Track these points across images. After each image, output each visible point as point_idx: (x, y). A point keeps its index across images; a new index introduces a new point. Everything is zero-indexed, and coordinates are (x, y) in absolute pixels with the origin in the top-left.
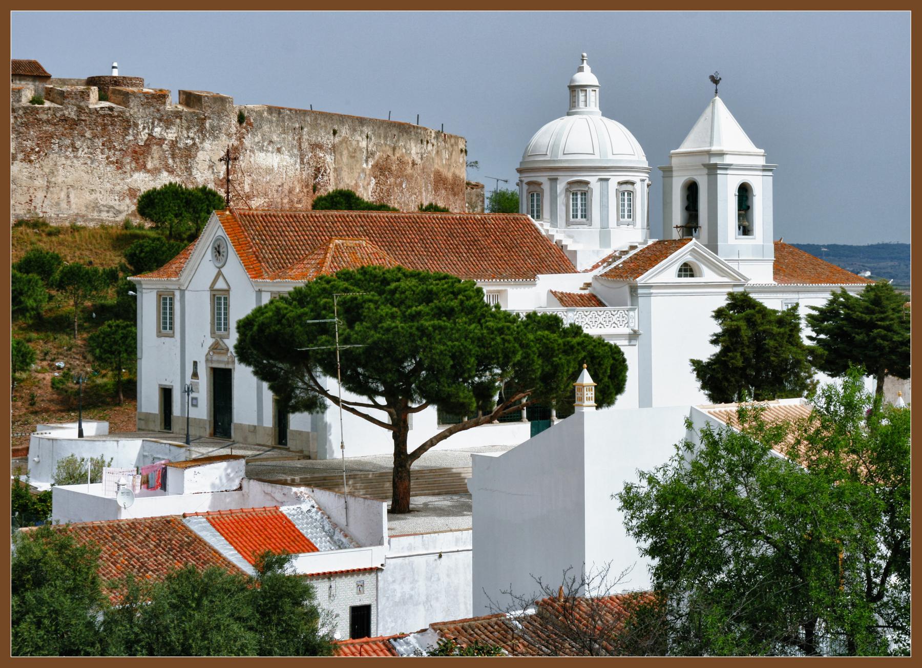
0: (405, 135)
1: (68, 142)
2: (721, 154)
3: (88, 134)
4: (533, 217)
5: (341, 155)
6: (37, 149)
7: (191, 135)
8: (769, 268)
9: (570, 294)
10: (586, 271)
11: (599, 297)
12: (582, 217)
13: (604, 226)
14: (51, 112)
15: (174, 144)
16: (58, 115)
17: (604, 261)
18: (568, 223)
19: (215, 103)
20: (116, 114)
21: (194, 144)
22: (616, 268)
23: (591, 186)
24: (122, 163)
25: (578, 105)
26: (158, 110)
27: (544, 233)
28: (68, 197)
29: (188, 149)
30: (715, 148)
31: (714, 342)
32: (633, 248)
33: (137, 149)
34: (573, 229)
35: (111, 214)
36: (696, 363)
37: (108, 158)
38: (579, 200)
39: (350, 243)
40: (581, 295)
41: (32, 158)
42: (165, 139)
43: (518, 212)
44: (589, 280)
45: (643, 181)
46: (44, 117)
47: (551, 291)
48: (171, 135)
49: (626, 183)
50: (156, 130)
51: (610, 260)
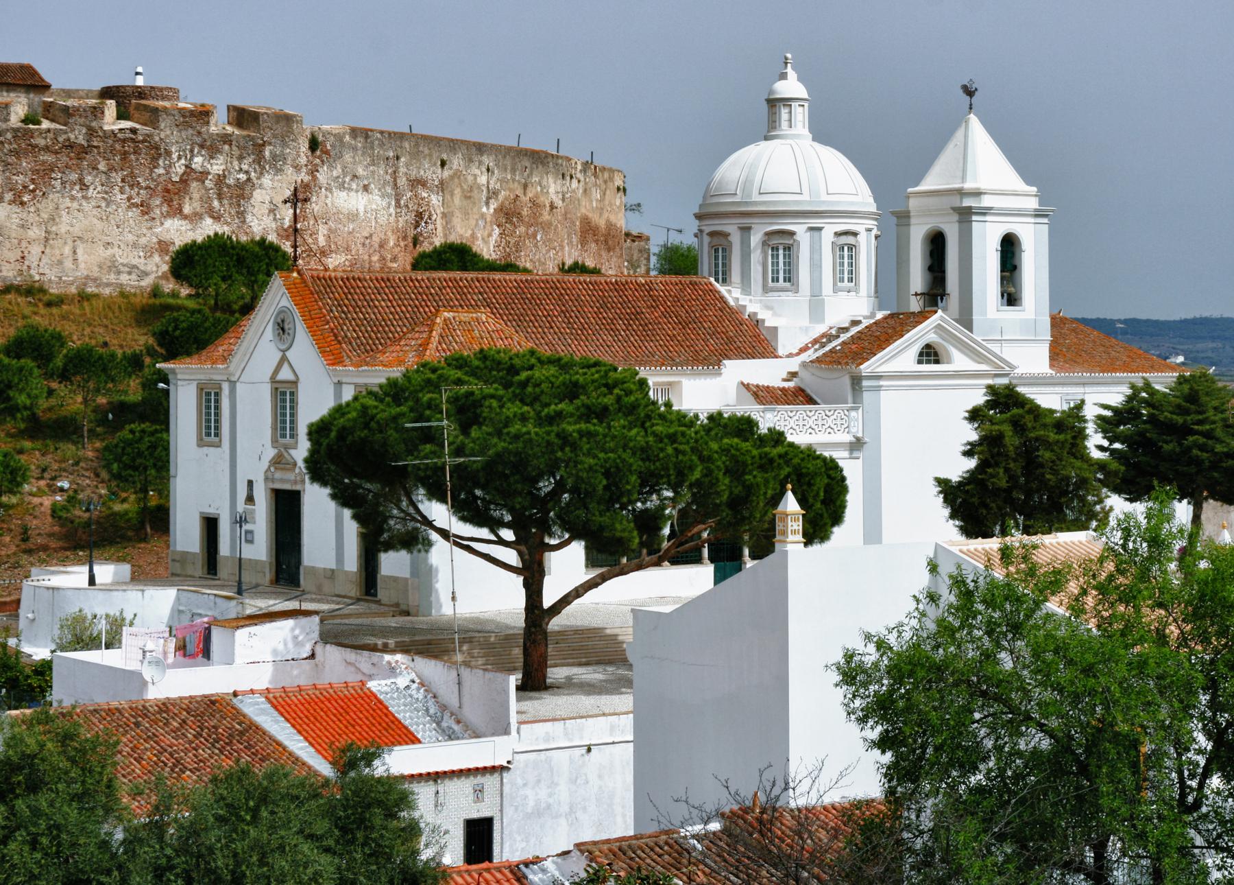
1: (74, 176)
2: (978, 194)
3: (102, 166)
4: (717, 280)
5: (452, 195)
6: (32, 187)
7: (245, 167)
8: (1043, 351)
9: (768, 387)
10: (790, 355)
11: (809, 391)
12: (785, 281)
13: (816, 294)
14: (51, 135)
15: (220, 180)
16: (61, 139)
17: (815, 342)
18: (766, 289)
19: (277, 122)
21: (249, 179)
22: (832, 351)
23: (797, 237)
24: (148, 206)
25: (780, 126)
26: (199, 133)
27: (732, 303)
28: (75, 252)
29: (240, 186)
30: (969, 185)
32: (855, 323)
33: (170, 186)
34: (773, 297)
37: (129, 199)
38: (781, 257)
39: (465, 316)
40: (784, 388)
41: (25, 199)
42: (209, 173)
43: (696, 274)
44: (795, 369)
45: (869, 230)
46: (41, 142)
47: (747, 387)
48: (217, 167)
49: (846, 233)
50: (196, 160)
51: (824, 340)
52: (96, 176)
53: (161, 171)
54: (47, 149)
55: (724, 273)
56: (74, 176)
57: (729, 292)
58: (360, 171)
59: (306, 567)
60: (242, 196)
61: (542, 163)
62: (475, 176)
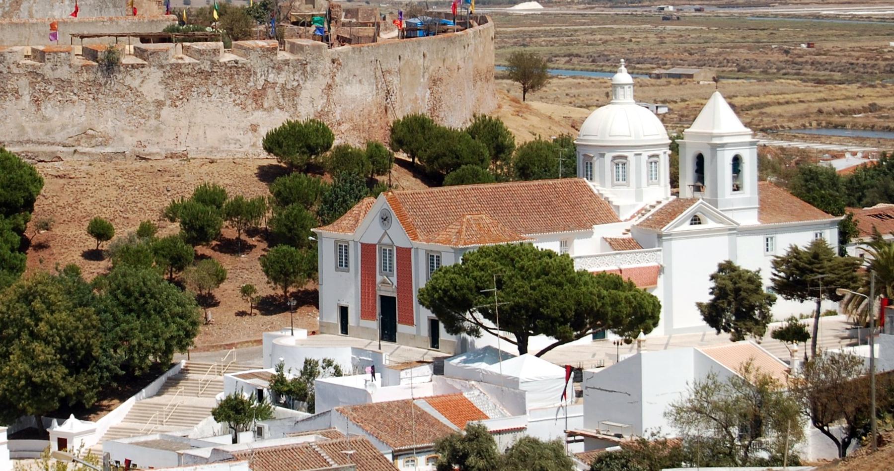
0: (452, 44)
1: (204, 89)
2: (721, 136)
3: (219, 83)
5: (405, 74)
6: (181, 97)
7: (296, 78)
8: (755, 213)
10: (626, 220)
13: (638, 186)
14: (191, 66)
15: (283, 87)
16: (196, 69)
17: (638, 212)
18: (613, 185)
19: (314, 50)
20: (240, 66)
22: (648, 219)
23: (628, 159)
24: (245, 104)
26: (272, 60)
27: (596, 192)
29: (294, 89)
30: (716, 131)
31: (711, 293)
33: (257, 93)
34: (617, 189)
35: (238, 146)
36: (700, 305)
37: (234, 101)
38: (620, 169)
39: (476, 217)
41: (177, 104)
44: (629, 228)
45: (665, 153)
46: (186, 71)
47: (606, 239)
48: (281, 79)
49: (653, 156)
50: (270, 76)
52: (216, 89)
53: (252, 84)
54: (189, 74)
55: (591, 175)
56: (204, 89)
57: (594, 186)
58: (357, 72)
59: (400, 333)
60: (295, 95)
61: (453, 42)
62: (417, 61)
